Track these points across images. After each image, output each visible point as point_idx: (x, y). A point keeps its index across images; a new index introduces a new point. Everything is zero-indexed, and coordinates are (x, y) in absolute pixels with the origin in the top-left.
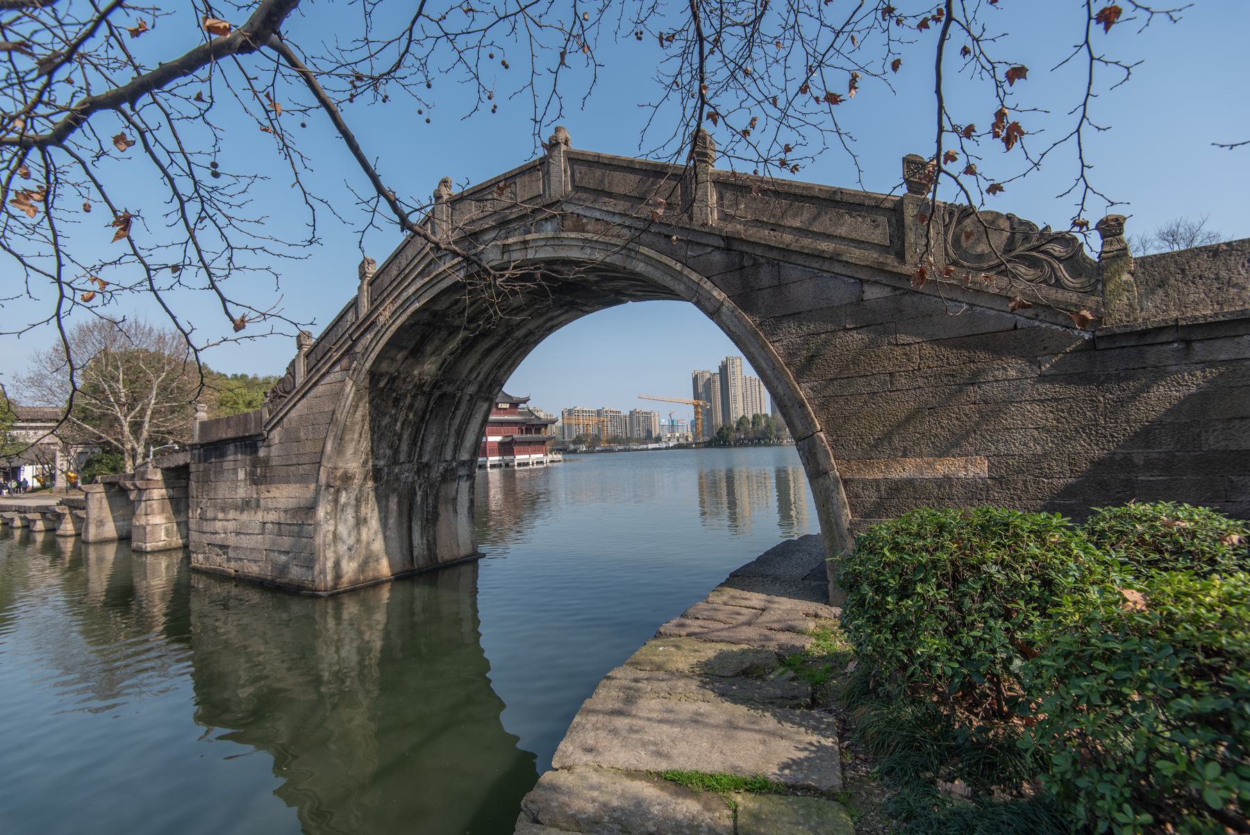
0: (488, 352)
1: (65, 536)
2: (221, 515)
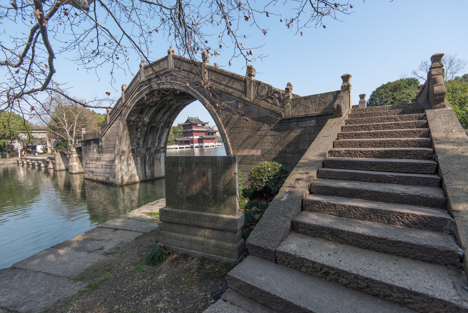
0: (165, 113)
1: (50, 169)
2: (91, 163)
